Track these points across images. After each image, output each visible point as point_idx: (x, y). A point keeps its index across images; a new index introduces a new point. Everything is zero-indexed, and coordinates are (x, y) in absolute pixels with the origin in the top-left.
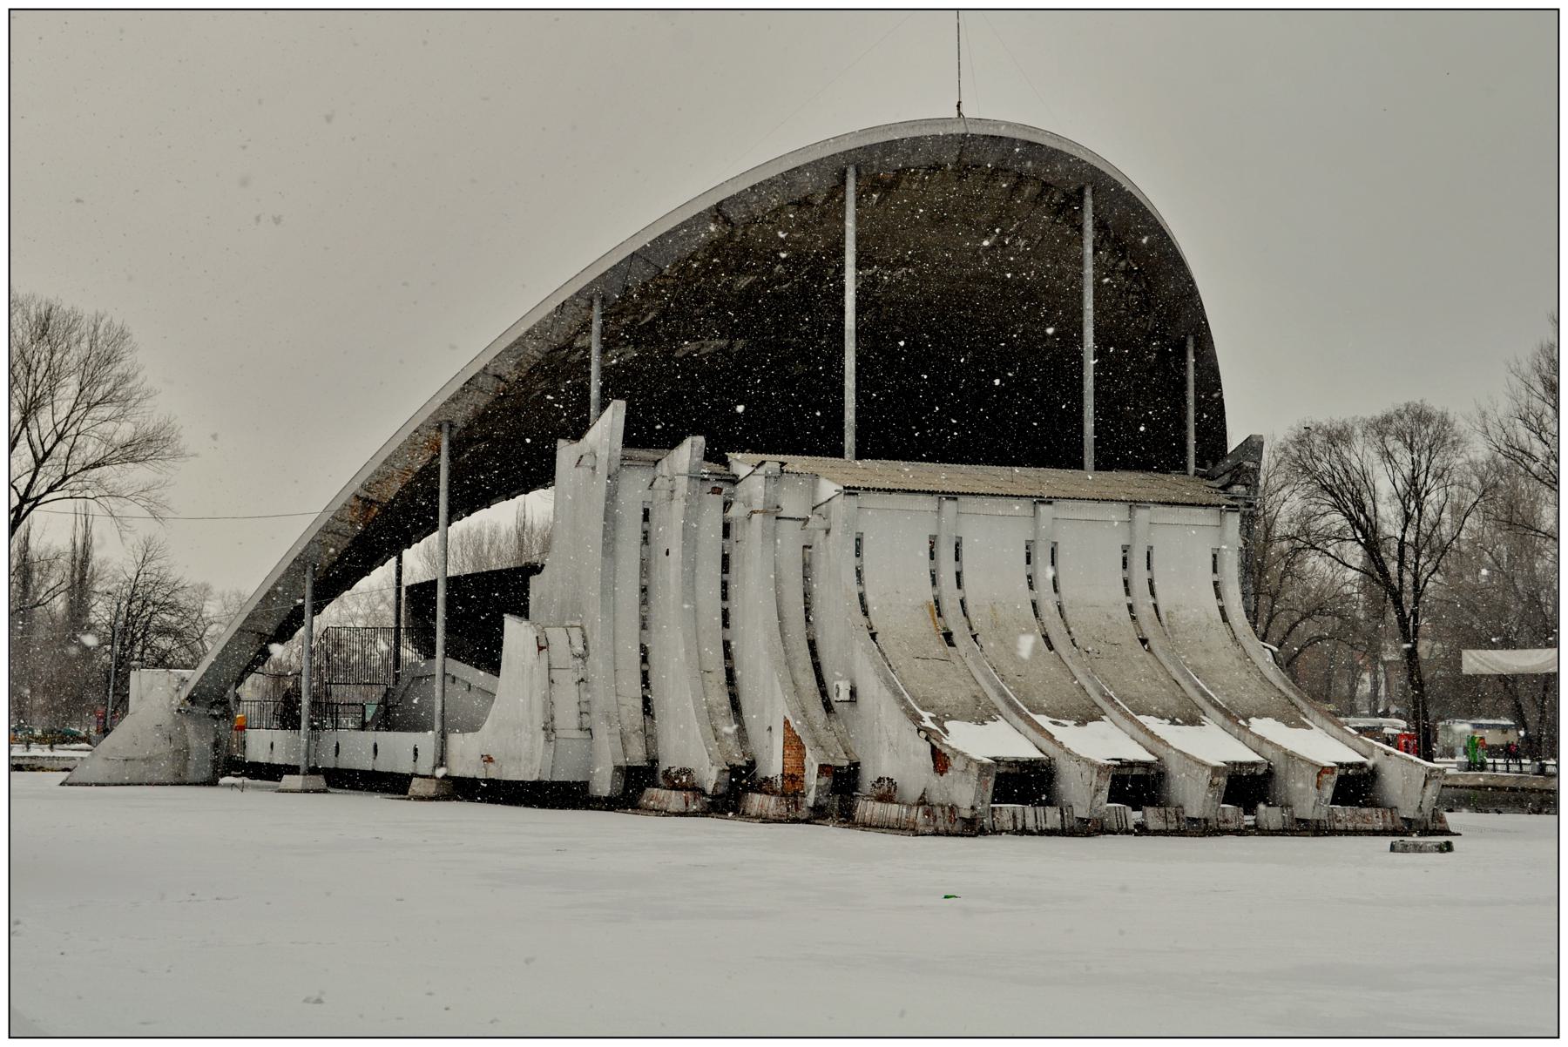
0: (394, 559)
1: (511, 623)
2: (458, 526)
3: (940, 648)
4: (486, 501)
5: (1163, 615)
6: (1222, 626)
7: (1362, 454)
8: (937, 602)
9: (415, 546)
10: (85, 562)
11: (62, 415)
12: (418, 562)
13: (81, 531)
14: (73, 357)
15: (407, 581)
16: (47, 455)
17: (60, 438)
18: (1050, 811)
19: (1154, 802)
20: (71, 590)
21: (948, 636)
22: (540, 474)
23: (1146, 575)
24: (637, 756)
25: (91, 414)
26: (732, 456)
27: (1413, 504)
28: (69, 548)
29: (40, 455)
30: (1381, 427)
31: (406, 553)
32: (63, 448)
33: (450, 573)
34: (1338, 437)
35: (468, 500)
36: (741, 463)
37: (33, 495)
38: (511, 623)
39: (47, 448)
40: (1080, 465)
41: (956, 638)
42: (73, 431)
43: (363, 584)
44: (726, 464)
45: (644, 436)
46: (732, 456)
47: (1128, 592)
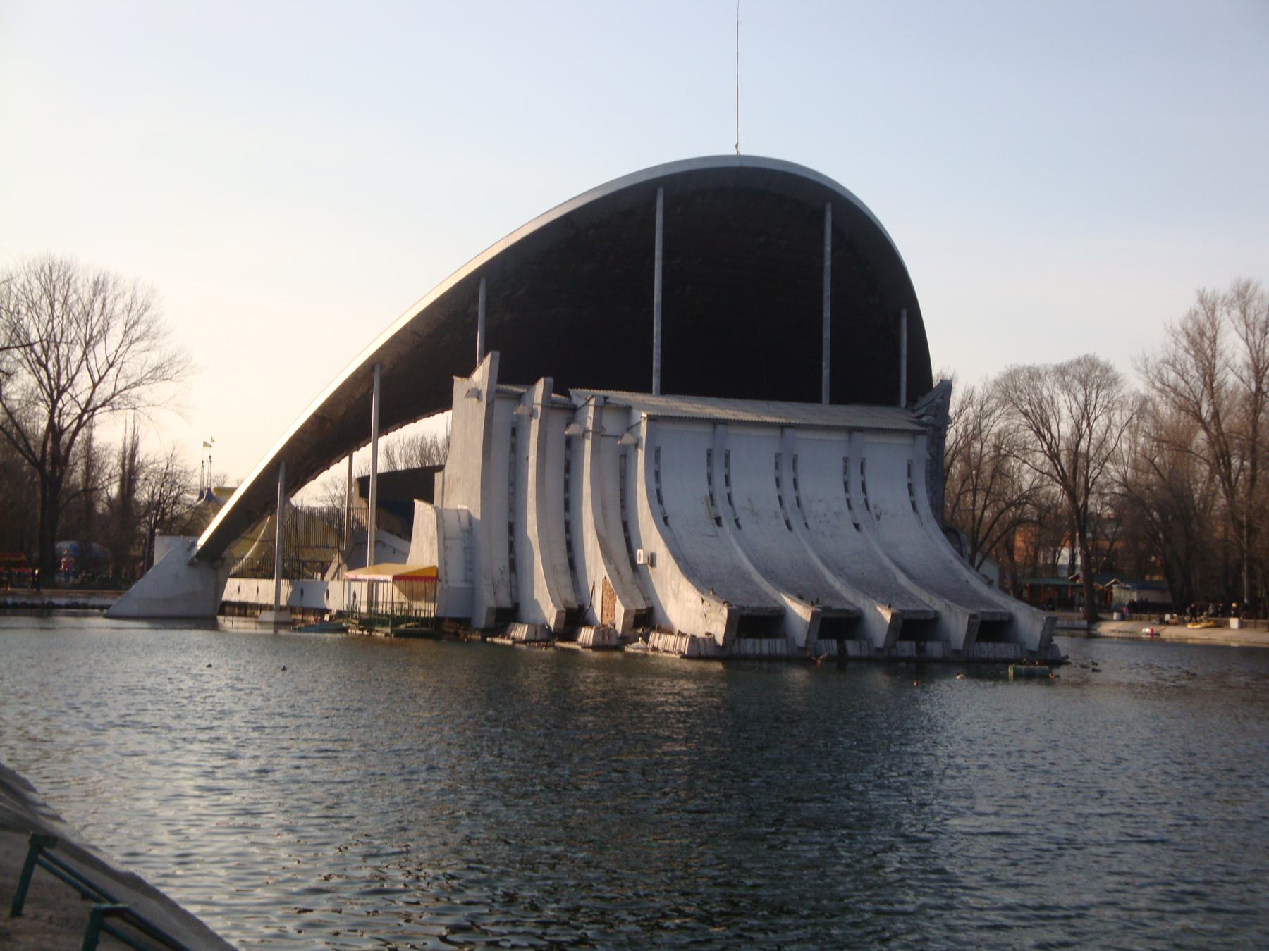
0: (347, 458)
1: (419, 506)
2: (383, 441)
3: (710, 528)
4: (412, 417)
5: (871, 506)
6: (912, 515)
7: (1048, 388)
8: (711, 496)
9: (362, 449)
10: (133, 456)
11: (111, 350)
12: (362, 460)
13: (130, 434)
14: (119, 307)
15: (356, 475)
16: (101, 379)
17: (111, 366)
18: (779, 642)
19: (1007, 640)
20: (122, 480)
21: (718, 521)
22: (442, 402)
23: (860, 479)
24: (505, 602)
25: (132, 347)
26: (572, 391)
27: (1085, 425)
28: (121, 446)
29: (97, 379)
30: (1061, 371)
31: (355, 454)
32: (113, 371)
33: (379, 471)
34: (1034, 375)
35: (394, 418)
36: (579, 395)
37: (91, 407)
38: (419, 506)
39: (102, 374)
40: (819, 400)
41: (724, 521)
42: (120, 361)
43: (325, 476)
44: (568, 395)
45: (513, 374)
46: (572, 391)
47: (846, 490)
